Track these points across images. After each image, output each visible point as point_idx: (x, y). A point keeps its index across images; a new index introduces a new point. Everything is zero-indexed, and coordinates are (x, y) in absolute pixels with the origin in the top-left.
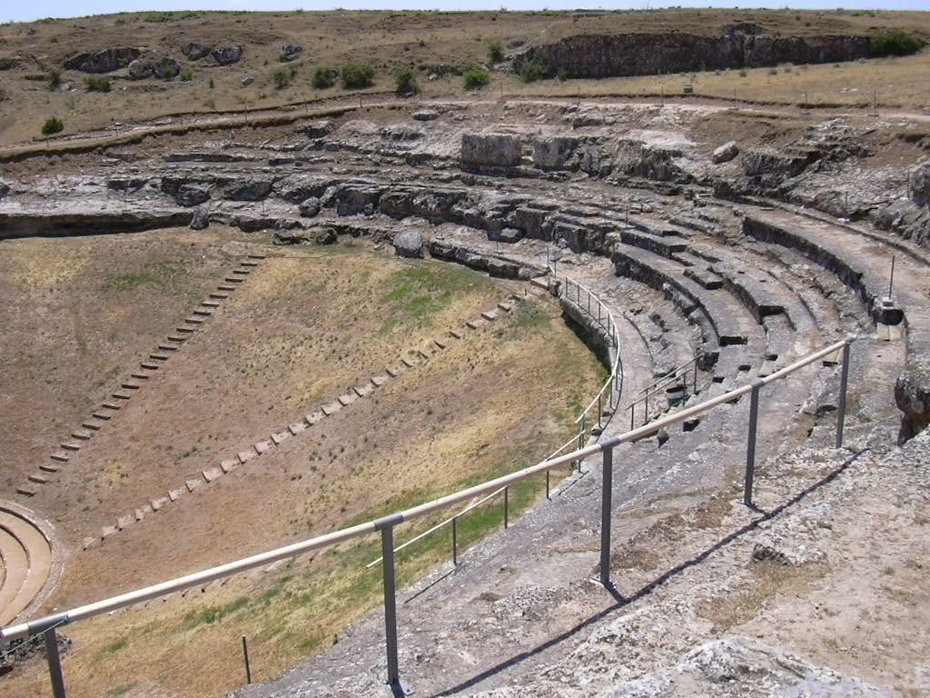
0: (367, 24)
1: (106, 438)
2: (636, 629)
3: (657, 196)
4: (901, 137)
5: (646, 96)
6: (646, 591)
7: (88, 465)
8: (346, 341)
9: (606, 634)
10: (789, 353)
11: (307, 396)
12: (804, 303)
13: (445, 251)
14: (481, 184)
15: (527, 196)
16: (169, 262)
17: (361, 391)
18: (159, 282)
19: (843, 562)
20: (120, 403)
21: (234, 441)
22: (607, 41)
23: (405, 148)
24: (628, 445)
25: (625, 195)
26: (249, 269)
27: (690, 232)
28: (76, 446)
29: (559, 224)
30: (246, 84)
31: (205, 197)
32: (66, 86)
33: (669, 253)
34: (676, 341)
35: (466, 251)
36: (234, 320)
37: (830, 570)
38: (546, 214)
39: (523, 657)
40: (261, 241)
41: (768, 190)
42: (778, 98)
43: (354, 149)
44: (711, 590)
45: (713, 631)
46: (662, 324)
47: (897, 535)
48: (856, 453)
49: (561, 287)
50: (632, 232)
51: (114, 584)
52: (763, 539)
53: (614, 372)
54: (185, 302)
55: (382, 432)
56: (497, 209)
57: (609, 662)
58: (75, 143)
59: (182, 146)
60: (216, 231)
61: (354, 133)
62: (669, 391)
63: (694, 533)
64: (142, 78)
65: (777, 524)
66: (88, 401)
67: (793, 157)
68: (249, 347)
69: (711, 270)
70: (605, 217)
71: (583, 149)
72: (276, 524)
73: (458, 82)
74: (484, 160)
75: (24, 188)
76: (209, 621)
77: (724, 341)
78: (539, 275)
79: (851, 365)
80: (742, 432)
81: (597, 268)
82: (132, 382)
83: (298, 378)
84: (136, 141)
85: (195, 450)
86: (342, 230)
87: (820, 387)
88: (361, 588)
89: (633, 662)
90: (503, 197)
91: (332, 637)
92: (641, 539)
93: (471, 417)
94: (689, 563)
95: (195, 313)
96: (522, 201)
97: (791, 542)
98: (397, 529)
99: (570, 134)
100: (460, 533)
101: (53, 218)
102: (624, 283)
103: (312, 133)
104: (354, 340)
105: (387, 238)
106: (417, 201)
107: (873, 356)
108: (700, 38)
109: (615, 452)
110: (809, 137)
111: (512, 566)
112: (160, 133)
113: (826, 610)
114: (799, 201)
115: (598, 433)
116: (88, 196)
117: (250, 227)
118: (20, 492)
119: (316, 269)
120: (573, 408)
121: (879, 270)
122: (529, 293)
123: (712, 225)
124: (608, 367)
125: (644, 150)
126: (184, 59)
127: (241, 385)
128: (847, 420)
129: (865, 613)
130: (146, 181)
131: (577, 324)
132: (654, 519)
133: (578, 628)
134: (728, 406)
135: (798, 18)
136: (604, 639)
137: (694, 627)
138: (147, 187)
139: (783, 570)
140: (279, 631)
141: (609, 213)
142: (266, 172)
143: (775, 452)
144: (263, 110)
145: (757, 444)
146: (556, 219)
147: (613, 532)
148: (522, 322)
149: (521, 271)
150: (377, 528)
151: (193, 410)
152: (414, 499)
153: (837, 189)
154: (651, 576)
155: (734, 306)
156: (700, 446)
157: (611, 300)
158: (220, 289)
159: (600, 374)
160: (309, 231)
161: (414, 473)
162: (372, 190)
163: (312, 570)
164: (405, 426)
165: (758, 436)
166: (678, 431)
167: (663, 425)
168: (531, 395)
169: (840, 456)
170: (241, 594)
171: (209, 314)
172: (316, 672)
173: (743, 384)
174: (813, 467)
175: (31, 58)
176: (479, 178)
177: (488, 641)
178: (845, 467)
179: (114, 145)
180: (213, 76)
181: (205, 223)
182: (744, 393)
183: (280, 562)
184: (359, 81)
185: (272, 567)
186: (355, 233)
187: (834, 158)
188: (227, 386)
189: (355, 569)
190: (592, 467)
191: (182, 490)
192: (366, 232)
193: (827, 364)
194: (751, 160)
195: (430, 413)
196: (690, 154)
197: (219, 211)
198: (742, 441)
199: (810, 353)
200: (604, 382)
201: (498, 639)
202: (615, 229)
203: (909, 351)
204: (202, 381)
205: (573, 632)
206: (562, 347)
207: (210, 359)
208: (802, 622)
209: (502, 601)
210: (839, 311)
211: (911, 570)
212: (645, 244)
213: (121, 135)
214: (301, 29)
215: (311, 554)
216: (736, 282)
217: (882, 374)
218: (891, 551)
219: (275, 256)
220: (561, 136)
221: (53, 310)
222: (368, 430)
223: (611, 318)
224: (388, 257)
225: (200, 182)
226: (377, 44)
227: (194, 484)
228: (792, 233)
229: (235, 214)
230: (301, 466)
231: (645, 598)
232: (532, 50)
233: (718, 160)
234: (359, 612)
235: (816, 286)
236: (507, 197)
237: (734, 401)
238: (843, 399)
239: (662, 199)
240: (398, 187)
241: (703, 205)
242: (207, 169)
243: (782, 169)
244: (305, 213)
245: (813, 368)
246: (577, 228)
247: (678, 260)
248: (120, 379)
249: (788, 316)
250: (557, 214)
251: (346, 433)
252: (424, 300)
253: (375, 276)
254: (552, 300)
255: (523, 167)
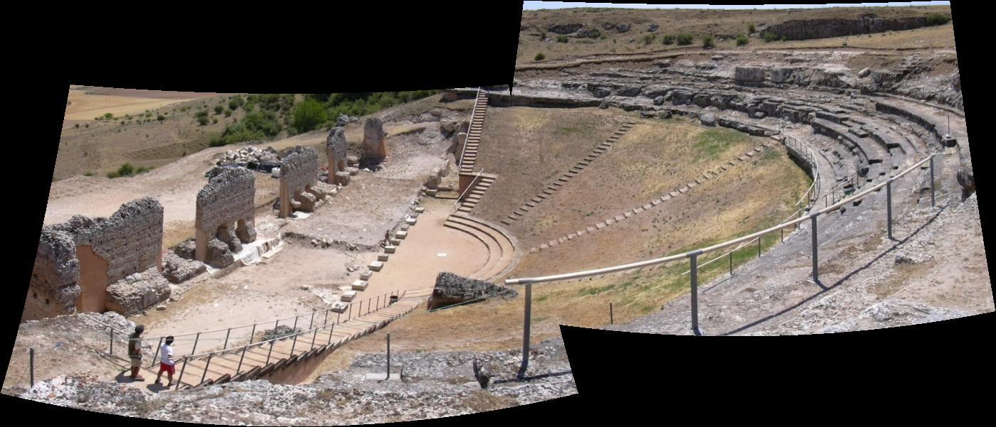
0: (690, 15)
1: (548, 203)
2: (834, 301)
3: (833, 95)
4: (945, 61)
5: (825, 48)
6: (839, 283)
7: (538, 215)
8: (674, 166)
9: (818, 305)
10: (904, 165)
11: (653, 191)
12: (908, 141)
13: (727, 123)
14: (745, 90)
15: (767, 96)
16: (587, 123)
17: (682, 190)
18: (582, 132)
19: (942, 259)
20: (557, 187)
21: (613, 211)
22: (805, 23)
23: (707, 73)
24: (824, 215)
25: (817, 95)
26: (627, 129)
27: (850, 111)
28: (533, 205)
29: (784, 109)
30: (631, 42)
31: (608, 94)
32: (548, 39)
33: (840, 121)
34: (846, 163)
35: (737, 123)
36: (618, 153)
37: (936, 263)
38: (777, 105)
39: (770, 317)
40: (634, 116)
41: (886, 89)
42: (887, 46)
43: (682, 74)
44: (874, 280)
45: (877, 299)
46: (839, 156)
47: (968, 243)
48: (942, 208)
49: (786, 140)
50: (821, 112)
51: (544, 271)
52: (900, 253)
53: (815, 180)
54: (594, 143)
55: (692, 210)
56: (753, 103)
57: (820, 318)
58: (549, 65)
59: (599, 69)
60: (612, 110)
61: (682, 66)
62: (845, 188)
63: (863, 254)
64: (583, 37)
65: (907, 246)
66: (541, 185)
67: (896, 73)
68: (624, 166)
69: (862, 128)
70: (807, 105)
71: (795, 73)
72: (632, 252)
73: (733, 42)
74: (746, 79)
75: (524, 84)
76: (592, 294)
77: (871, 162)
78: (775, 134)
79: (935, 168)
80: (884, 205)
81: (804, 130)
82: (564, 178)
83: (649, 183)
84: (577, 66)
85: (592, 213)
86: (674, 112)
87: (921, 179)
88: (678, 285)
89: (834, 317)
90: (756, 97)
91: (660, 307)
92: (834, 259)
93: (740, 204)
94: (861, 269)
95: (599, 148)
96: (765, 99)
97: (915, 253)
98: (699, 257)
99: (788, 66)
100: (733, 260)
101: (535, 98)
102: (819, 137)
103: (662, 65)
104: (679, 165)
105: (697, 116)
106: (713, 99)
107: (945, 162)
108: (848, 21)
109: (818, 219)
110: (903, 64)
111: (763, 275)
112: (589, 63)
113: (936, 282)
114: (901, 93)
115: (808, 210)
116: (553, 90)
117: (629, 109)
118: (503, 222)
119: (661, 130)
120: (794, 198)
121: (943, 122)
122: (770, 143)
123: (861, 107)
124: (812, 178)
125: (825, 73)
126: (603, 29)
127: (619, 184)
128: (936, 193)
129: (957, 280)
130: (580, 85)
131: (794, 157)
132: (841, 249)
133: (802, 303)
134: (876, 193)
135: (893, 10)
136: (817, 307)
137: (867, 298)
138: (580, 87)
139: (912, 267)
140: (630, 302)
141: (809, 104)
142: (638, 83)
143: (901, 212)
144: (638, 54)
145: (892, 209)
146: (783, 107)
147: (819, 257)
148: (767, 157)
149: (765, 133)
150: (688, 256)
151: (593, 194)
152: (709, 243)
153: (919, 87)
154: (841, 277)
155: (875, 145)
156: (863, 213)
157: (812, 146)
158: (612, 137)
159: (808, 181)
160: (658, 112)
161: (709, 231)
162: (690, 93)
163: (651, 274)
164: (705, 207)
165: (892, 206)
166: (851, 206)
167: (842, 204)
168: (772, 192)
169: (935, 210)
170: (611, 283)
171: (605, 149)
172: (650, 322)
173: (882, 182)
174: (921, 217)
175: (534, 26)
176: (744, 88)
177: (750, 311)
178: (937, 215)
179: (567, 67)
180: (616, 38)
181: (607, 106)
182: (883, 186)
183: (633, 270)
184: (685, 41)
185: (629, 272)
186: (681, 114)
187: (915, 73)
188: (612, 184)
189: (675, 275)
190: (806, 227)
191: (584, 231)
192: (686, 113)
193: (923, 168)
194: (877, 76)
195: (718, 201)
196: (847, 74)
197: (614, 101)
198: (884, 209)
199: (914, 164)
200: (811, 185)
201: (756, 309)
202: (812, 111)
203: (961, 158)
204: (599, 181)
205: (799, 305)
206: (788, 169)
207: (604, 170)
208: (925, 289)
209: (758, 291)
210: (926, 143)
211: (976, 257)
212: (828, 118)
213: (571, 63)
214: (659, 17)
215: (651, 267)
216: (874, 133)
217: (949, 170)
218: (965, 250)
219: (640, 123)
220: (784, 67)
221: (530, 141)
222: (685, 208)
223: (813, 154)
224: (697, 125)
225: (606, 86)
226: (695, 25)
227: (591, 229)
228: (899, 108)
229: (622, 102)
230: (648, 225)
231: (839, 286)
232: (769, 27)
233: (861, 77)
234: (677, 295)
235: (914, 133)
236: (758, 96)
237: (878, 190)
238: (933, 184)
239: (836, 96)
240: (703, 92)
241: (855, 98)
242: (610, 81)
243: (892, 79)
244: (656, 103)
245: (917, 171)
246: (794, 111)
247: (845, 125)
248: (558, 176)
249: (901, 148)
250: (783, 104)
251: (673, 210)
252: (716, 146)
253: (690, 135)
254: (782, 146)
255: (765, 82)
